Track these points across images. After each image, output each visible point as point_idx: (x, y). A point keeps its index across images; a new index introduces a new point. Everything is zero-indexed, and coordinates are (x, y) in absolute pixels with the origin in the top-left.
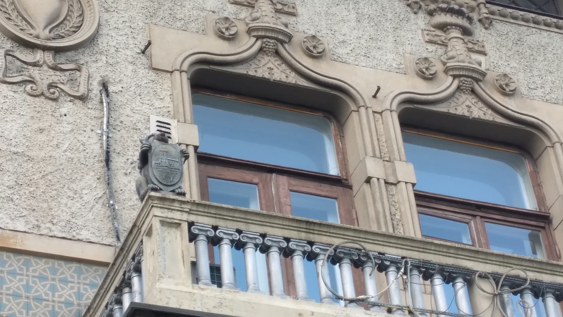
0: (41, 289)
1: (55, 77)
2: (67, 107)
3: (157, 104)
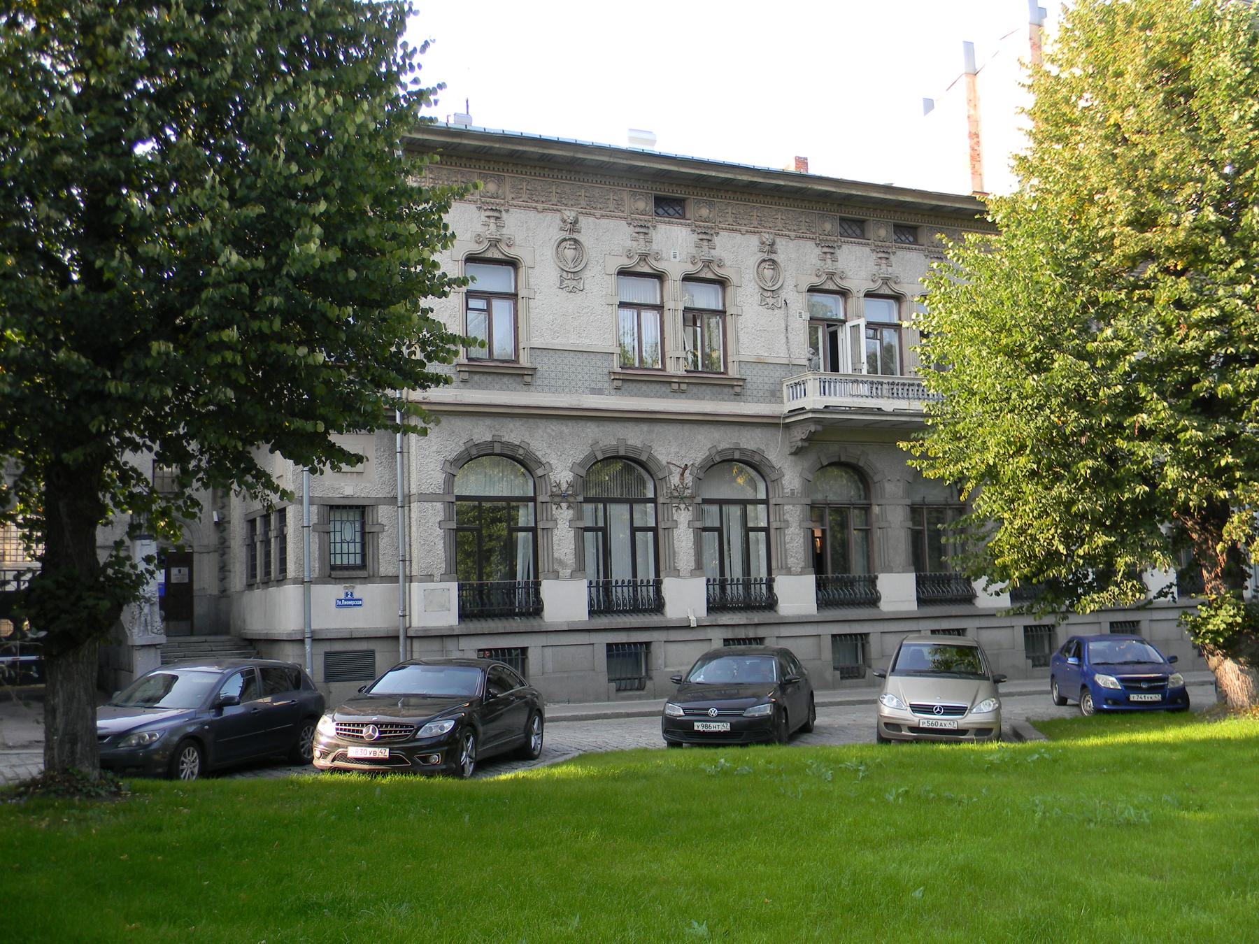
0: (599, 363)
1: (575, 283)
2: (776, 311)
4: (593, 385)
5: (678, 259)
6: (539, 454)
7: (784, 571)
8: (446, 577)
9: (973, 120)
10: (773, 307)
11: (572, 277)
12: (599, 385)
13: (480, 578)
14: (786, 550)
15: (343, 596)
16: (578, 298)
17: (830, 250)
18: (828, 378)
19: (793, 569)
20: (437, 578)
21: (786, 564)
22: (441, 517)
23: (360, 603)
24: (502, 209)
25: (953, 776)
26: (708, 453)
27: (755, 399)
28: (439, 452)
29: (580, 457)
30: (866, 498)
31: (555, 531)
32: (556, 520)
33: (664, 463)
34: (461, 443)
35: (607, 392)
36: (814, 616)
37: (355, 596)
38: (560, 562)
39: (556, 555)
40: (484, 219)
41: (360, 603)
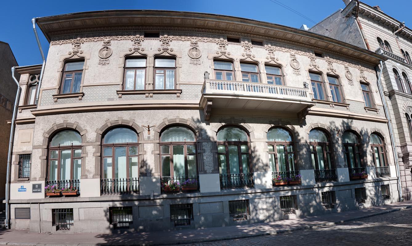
1: (197, 62)
3: (209, 64)
4: (109, 97)
5: (153, 50)
6: (82, 126)
7: (203, 172)
8: (41, 179)
9: (176, 244)
10: (196, 64)
11: (105, 59)
12: (112, 97)
13: (276, 171)
14: (204, 163)
15: (20, 188)
16: (106, 67)
17: (223, 46)
18: (226, 82)
19: (207, 171)
20: (37, 179)
21: (204, 169)
22: (41, 154)
23: (25, 190)
24: (226, 44)
25: (73, 40)
26: (162, 121)
27: (188, 98)
28: (42, 129)
29: (100, 126)
30: (370, 17)
31: (87, 158)
32: (87, 153)
33: (140, 126)
34: (51, 125)
35: (115, 99)
36: (218, 192)
37: (24, 188)
38: (88, 171)
39: (86, 168)
40: (74, 47)
41: (25, 190)
